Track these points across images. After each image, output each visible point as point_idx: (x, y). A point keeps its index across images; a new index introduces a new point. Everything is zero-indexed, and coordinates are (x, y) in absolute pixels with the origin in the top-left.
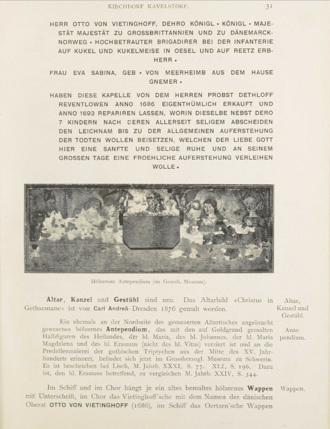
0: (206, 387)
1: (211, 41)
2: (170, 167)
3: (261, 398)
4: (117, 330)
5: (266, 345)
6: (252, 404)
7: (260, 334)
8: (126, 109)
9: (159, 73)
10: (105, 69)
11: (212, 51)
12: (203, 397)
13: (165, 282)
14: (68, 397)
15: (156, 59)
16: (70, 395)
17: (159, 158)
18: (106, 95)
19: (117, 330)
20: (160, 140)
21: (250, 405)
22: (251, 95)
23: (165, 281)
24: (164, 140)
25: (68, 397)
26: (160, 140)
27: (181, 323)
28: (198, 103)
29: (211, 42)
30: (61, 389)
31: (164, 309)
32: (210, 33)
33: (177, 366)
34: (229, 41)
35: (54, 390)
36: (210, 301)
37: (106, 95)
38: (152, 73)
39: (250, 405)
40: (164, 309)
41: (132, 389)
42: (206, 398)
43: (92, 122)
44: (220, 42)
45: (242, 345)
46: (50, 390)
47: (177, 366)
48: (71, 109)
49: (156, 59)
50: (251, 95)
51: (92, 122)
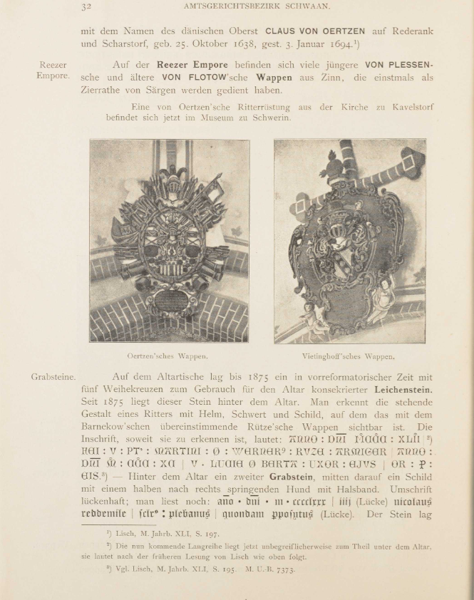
3: (281, 428)
4: (416, 391)
5: (378, 403)
6: (110, 387)
9: (384, 66)
10: (60, 382)
13: (85, 415)
14: (107, 439)
16: (110, 437)
19: (416, 391)
20: (347, 31)
21: (306, 425)
23: (34, 376)
25: (107, 439)
26: (347, 31)
27: (185, 514)
28: (87, 457)
30: (235, 416)
31: (252, 377)
35: (265, 406)
36: (296, 390)
38: (308, 31)
39: (306, 425)
40: (252, 377)
45: (298, 415)
46: (85, 443)
48: (362, 484)
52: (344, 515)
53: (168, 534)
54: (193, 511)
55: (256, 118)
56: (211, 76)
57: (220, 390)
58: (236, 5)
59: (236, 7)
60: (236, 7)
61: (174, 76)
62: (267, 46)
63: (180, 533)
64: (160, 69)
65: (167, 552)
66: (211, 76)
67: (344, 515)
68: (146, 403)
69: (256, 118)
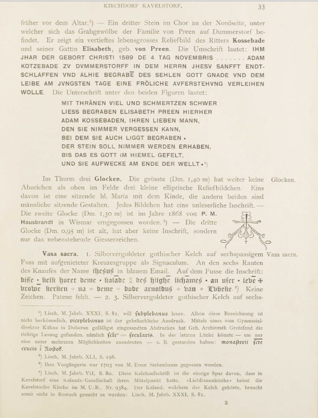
0: (101, 204)
1: (70, 137)
2: (38, 92)
7: (235, 36)
8: (173, 134)
11: (244, 75)
12: (71, 271)
13: (61, 50)
15: (90, 74)
16: (97, 91)
17: (87, 75)
18: (165, 129)
21: (71, 221)
22: (150, 112)
24: (177, 103)
29: (70, 138)
31: (171, 214)
32: (244, 75)
33: (184, 394)
34: (73, 146)
37: (165, 129)
39: (71, 221)
40: (171, 214)
41: (29, 205)
42: (218, 24)
43: (182, 66)
44: (64, 146)
47: (184, 394)
49: (90, 74)
50: (150, 112)
51: (182, 66)
52: (37, 231)
53: (56, 373)
54: (148, 291)
55: (252, 315)
56: (111, 66)
57: (135, 272)
58: (120, 5)
59: (120, 7)
60: (120, 7)
61: (136, 104)
62: (122, 50)
63: (98, 313)
64: (235, 43)
65: (144, 377)
66: (111, 66)
67: (74, 214)
68: (69, 42)
69: (252, 315)
